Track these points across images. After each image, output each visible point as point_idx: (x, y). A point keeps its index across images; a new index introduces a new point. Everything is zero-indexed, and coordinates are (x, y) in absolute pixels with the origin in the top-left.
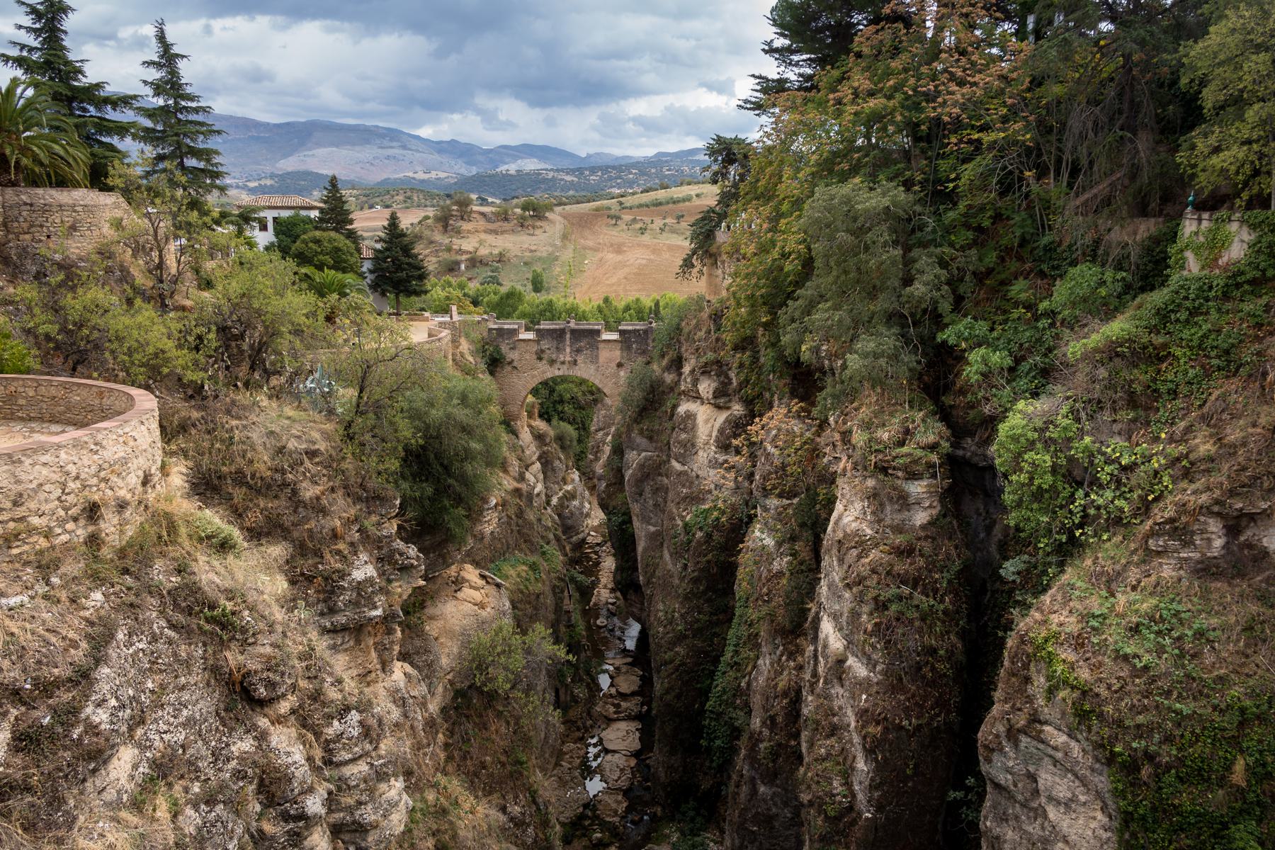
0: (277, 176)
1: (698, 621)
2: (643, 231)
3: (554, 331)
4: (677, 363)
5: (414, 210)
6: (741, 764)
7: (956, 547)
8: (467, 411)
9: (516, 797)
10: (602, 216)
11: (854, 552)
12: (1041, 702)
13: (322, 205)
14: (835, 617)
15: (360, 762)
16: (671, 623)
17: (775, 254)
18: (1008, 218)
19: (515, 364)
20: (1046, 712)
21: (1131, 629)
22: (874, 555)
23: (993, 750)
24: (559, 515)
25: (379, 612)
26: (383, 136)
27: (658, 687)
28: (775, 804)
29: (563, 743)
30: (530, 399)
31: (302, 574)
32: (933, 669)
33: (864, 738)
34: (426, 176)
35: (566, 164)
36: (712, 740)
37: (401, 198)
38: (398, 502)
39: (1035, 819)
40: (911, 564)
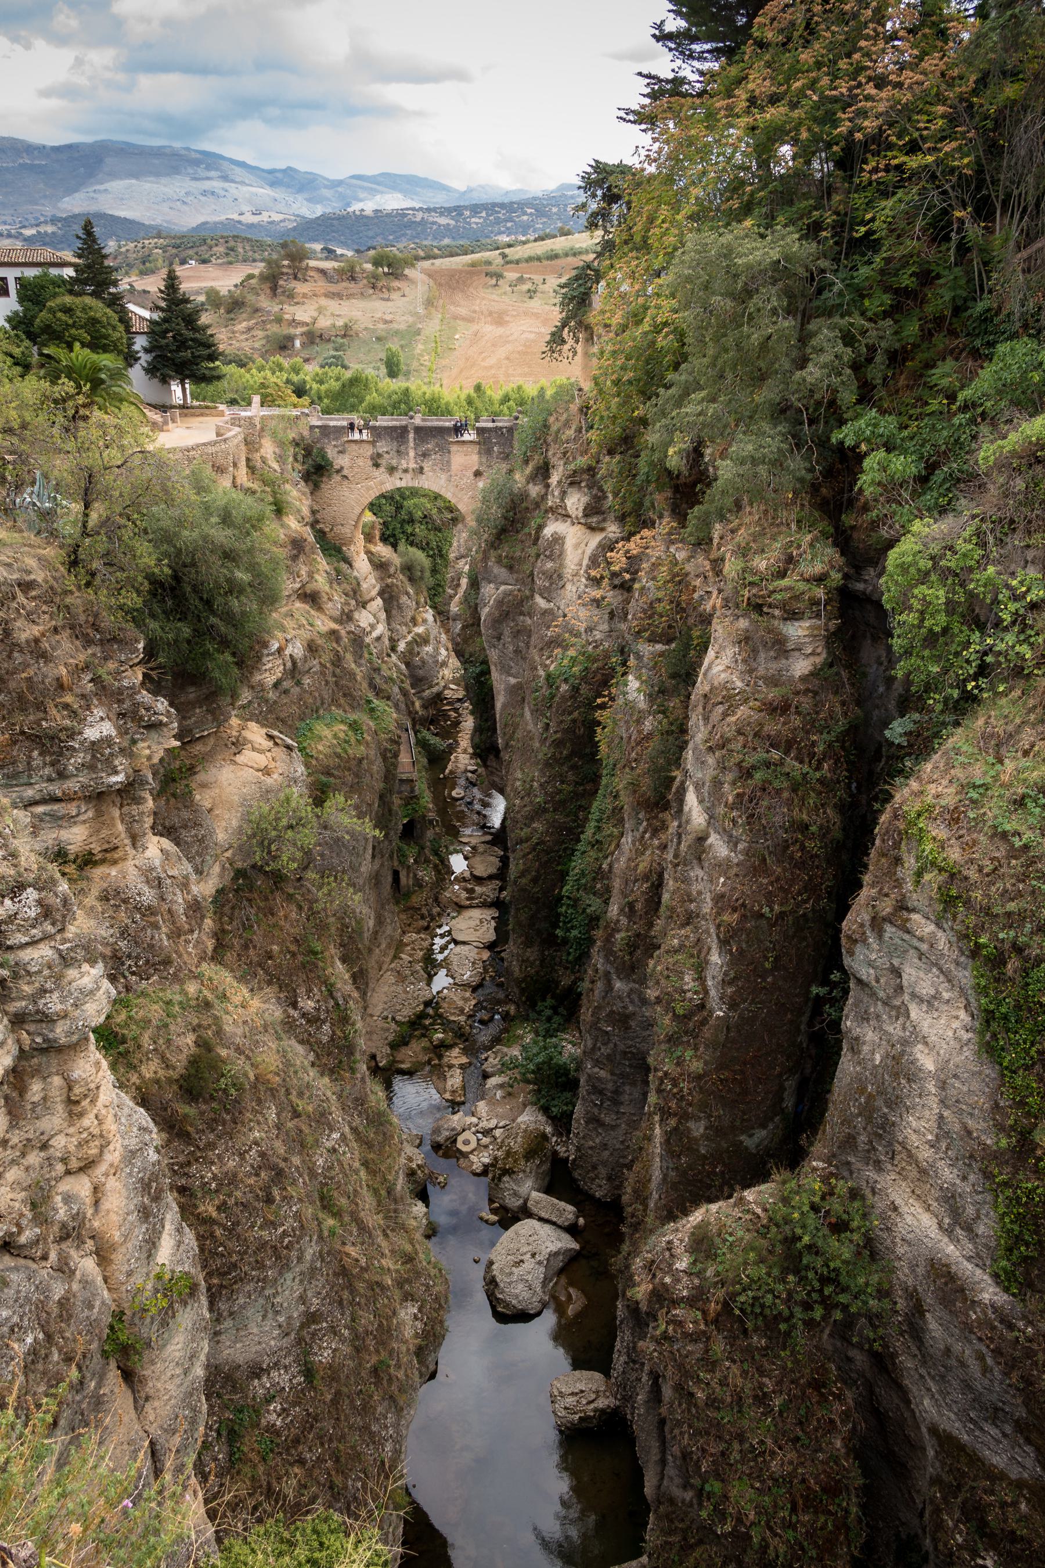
0: (60, 219)
1: (560, 791)
2: (531, 294)
3: (393, 429)
4: (543, 471)
5: (239, 266)
6: (598, 960)
7: (843, 703)
8: (229, 532)
9: (309, 990)
10: (480, 272)
11: (720, 709)
12: (909, 886)
13: (77, 260)
14: (698, 787)
15: (41, 946)
16: (529, 795)
17: (646, 326)
18: (938, 276)
19: (345, 472)
20: (916, 899)
21: (1015, 802)
22: (743, 712)
23: (856, 941)
24: (408, 664)
25: (120, 778)
26: (196, 163)
27: (513, 870)
28: (632, 1002)
29: (404, 932)
30: (369, 517)
31: (23, 733)
32: (803, 848)
33: (718, 926)
34: (255, 219)
35: (440, 200)
36: (568, 930)
37: (221, 249)
38: (141, 646)
39: (897, 1018)
40: (784, 724)
